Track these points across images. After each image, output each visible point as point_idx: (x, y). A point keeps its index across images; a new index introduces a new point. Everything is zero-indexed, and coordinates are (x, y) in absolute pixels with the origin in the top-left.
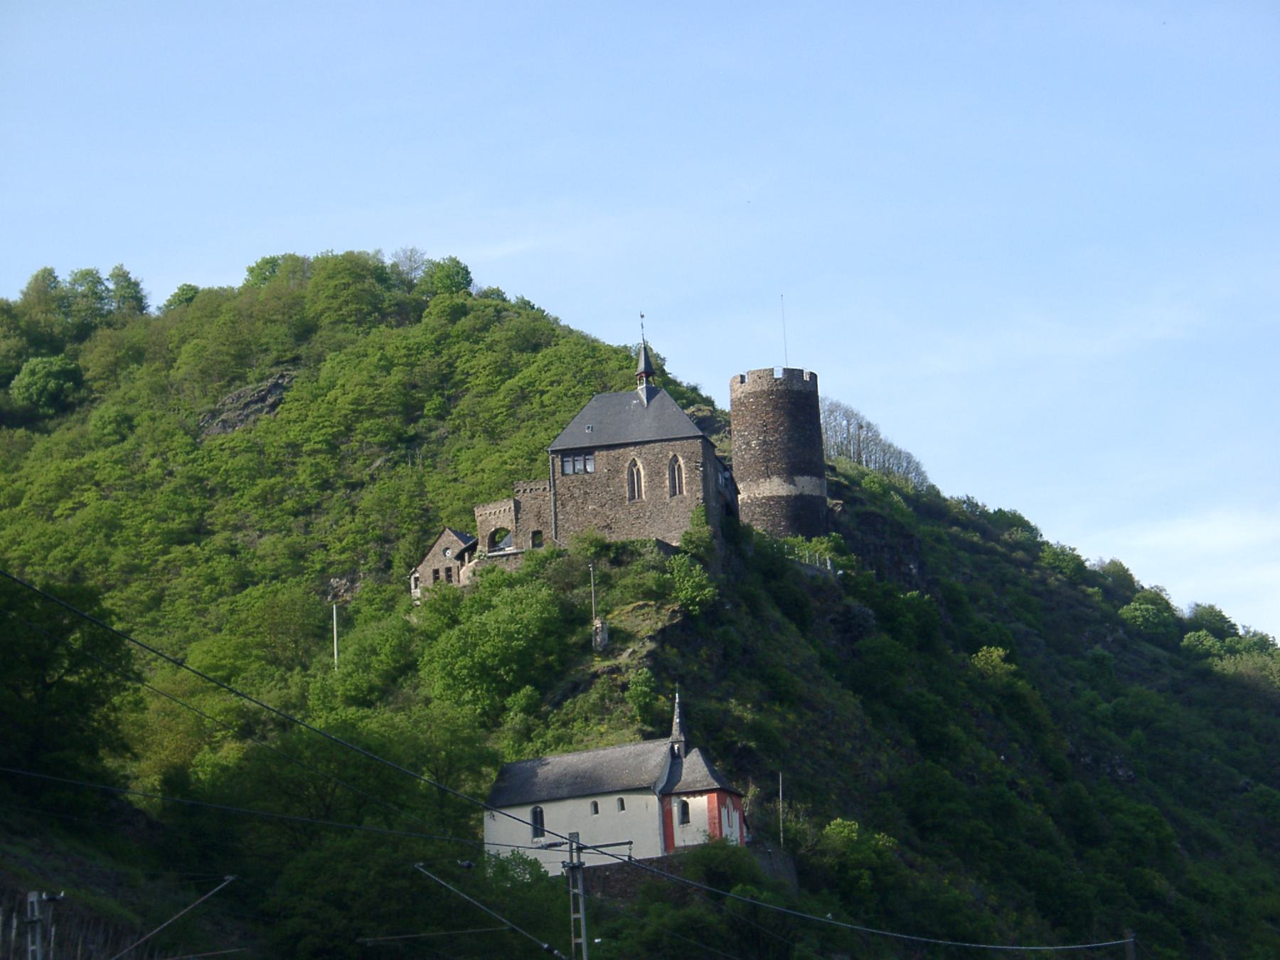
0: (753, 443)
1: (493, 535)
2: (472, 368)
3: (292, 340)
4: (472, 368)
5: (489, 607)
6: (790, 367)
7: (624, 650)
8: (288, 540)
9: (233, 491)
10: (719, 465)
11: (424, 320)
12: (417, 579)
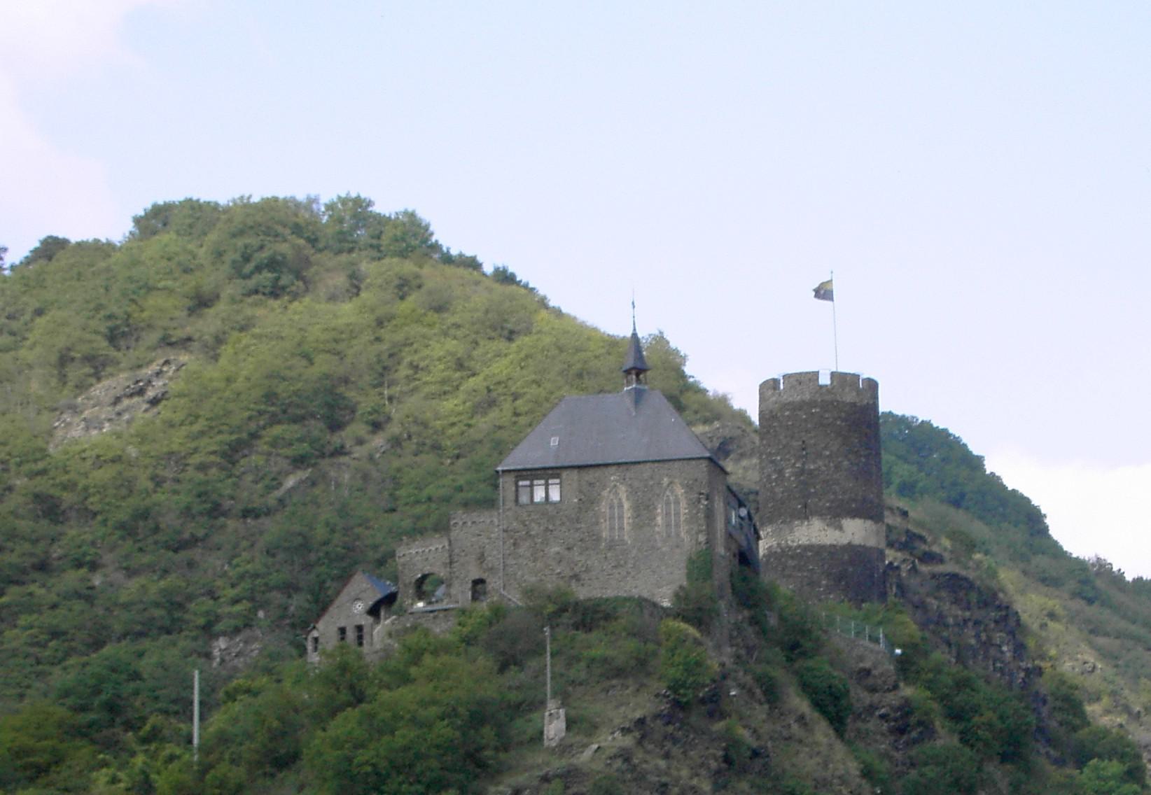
0: (788, 472)
1: (421, 582)
2: (423, 359)
3: (186, 313)
4: (423, 359)
5: (406, 680)
6: (841, 370)
7: (586, 746)
8: (162, 583)
9: (95, 514)
10: (732, 499)
11: (363, 295)
12: (316, 640)
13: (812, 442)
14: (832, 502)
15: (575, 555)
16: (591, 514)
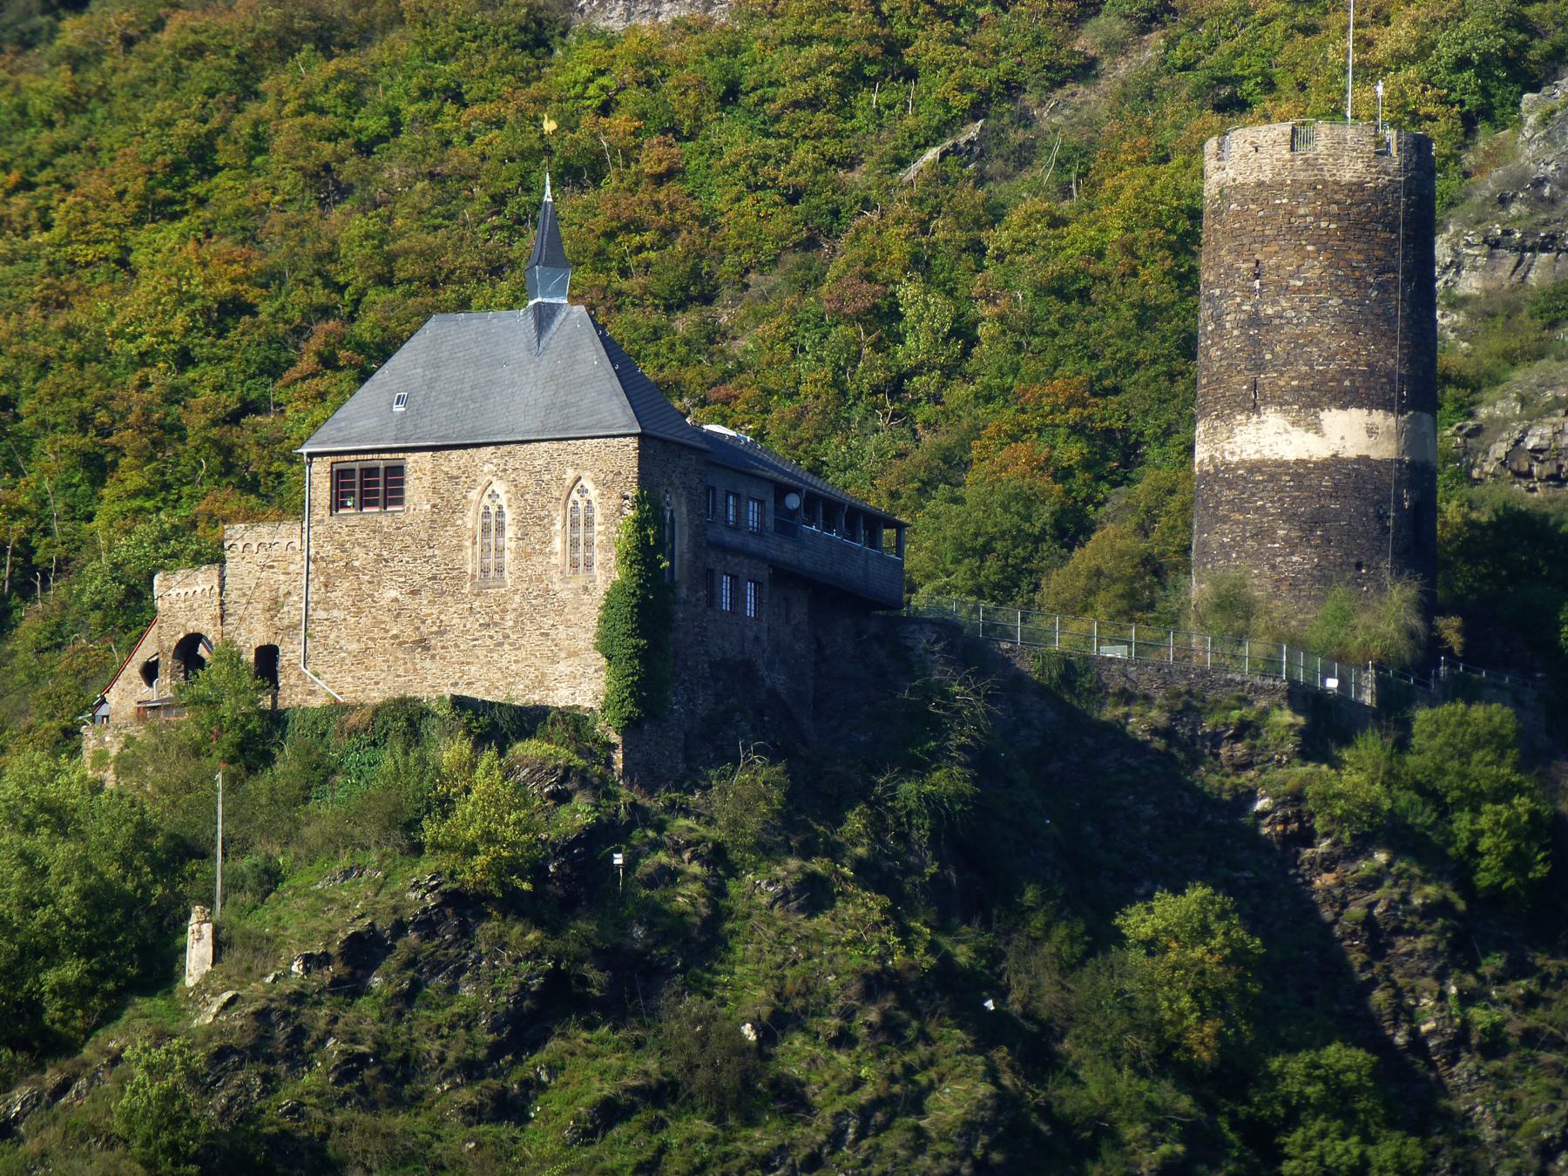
13: (1273, 262)
14: (1302, 378)
15: (423, 604)
16: (451, 530)
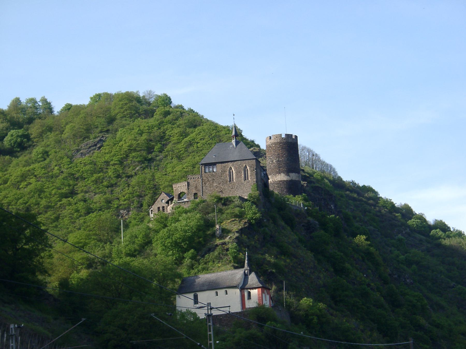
0: (274, 161)
1: (180, 194)
2: (172, 134)
3: (106, 124)
4: (172, 134)
5: (178, 221)
6: (288, 133)
7: (227, 236)
8: (105, 196)
9: (85, 179)
10: (262, 169)
11: (155, 116)
12: (152, 211)
